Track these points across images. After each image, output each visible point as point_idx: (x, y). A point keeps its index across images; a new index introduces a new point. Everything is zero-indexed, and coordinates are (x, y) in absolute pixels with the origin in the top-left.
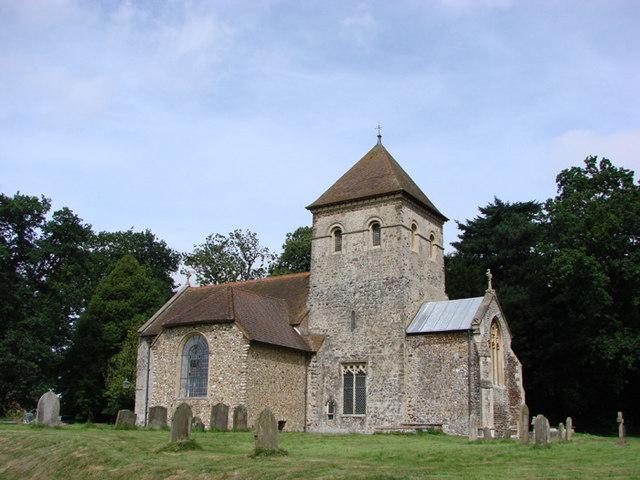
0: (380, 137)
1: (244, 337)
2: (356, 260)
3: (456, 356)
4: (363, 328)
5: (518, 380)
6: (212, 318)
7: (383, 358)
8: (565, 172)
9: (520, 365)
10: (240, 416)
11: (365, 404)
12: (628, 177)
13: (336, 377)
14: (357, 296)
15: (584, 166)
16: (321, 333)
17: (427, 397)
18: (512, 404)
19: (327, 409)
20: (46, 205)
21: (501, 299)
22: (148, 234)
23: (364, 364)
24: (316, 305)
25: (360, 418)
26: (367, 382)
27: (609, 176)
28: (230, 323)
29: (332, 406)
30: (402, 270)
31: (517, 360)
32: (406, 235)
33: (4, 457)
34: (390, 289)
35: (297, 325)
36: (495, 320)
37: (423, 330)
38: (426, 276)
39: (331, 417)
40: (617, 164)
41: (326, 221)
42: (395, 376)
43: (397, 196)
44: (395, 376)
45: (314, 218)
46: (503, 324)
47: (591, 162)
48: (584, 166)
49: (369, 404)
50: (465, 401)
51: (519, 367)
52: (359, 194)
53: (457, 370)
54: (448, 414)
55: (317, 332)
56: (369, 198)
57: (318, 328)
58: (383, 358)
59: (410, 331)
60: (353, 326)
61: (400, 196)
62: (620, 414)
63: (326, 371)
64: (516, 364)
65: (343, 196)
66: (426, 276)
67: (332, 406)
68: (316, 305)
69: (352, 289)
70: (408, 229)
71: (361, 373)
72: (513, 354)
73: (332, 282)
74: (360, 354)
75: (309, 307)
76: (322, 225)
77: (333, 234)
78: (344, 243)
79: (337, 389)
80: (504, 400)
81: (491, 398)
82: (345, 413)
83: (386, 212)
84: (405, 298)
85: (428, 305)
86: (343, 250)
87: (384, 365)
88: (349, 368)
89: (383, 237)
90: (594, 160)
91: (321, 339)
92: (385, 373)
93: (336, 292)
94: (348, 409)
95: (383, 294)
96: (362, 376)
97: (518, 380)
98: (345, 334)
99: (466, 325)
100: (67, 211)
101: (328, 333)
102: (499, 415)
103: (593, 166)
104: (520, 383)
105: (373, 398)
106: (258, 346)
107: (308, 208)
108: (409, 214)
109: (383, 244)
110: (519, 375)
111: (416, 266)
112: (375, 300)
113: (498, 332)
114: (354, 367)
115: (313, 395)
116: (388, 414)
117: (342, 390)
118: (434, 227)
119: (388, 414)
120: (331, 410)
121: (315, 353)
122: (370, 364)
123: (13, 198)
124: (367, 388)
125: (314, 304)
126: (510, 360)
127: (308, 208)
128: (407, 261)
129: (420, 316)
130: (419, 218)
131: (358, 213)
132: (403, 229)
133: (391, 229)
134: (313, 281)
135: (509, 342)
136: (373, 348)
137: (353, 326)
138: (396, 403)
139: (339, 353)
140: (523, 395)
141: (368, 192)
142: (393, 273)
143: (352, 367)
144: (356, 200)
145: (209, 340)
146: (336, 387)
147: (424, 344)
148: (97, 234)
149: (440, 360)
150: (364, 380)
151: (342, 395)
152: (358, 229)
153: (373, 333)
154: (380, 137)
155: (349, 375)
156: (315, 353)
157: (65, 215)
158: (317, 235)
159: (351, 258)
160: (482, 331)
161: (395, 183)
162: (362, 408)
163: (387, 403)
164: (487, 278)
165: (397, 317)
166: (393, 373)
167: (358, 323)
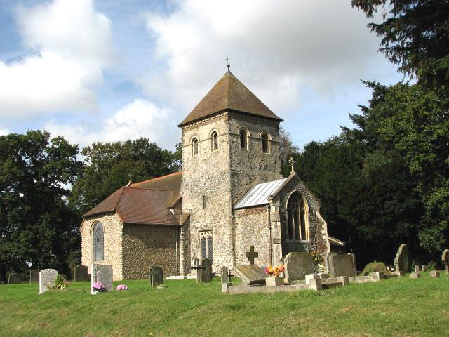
0: (228, 66)
2: (205, 160)
3: (262, 222)
4: (210, 206)
5: (324, 234)
7: (220, 226)
20: (48, 135)
28: (113, 213)
31: (323, 220)
33: (2, 305)
41: (189, 134)
52: (207, 113)
58: (220, 226)
60: (204, 206)
64: (323, 223)
89: (219, 143)
95: (220, 182)
96: (210, 238)
97: (324, 234)
98: (201, 211)
100: (60, 138)
107: (179, 126)
109: (219, 148)
122: (214, 231)
123: (25, 134)
125: (184, 193)
127: (179, 126)
134: (184, 177)
137: (204, 206)
139: (198, 225)
145: (104, 224)
147: (244, 215)
154: (228, 66)
155: (204, 239)
157: (59, 140)
158: (185, 144)
159: (203, 158)
163: (224, 257)
167: (207, 204)
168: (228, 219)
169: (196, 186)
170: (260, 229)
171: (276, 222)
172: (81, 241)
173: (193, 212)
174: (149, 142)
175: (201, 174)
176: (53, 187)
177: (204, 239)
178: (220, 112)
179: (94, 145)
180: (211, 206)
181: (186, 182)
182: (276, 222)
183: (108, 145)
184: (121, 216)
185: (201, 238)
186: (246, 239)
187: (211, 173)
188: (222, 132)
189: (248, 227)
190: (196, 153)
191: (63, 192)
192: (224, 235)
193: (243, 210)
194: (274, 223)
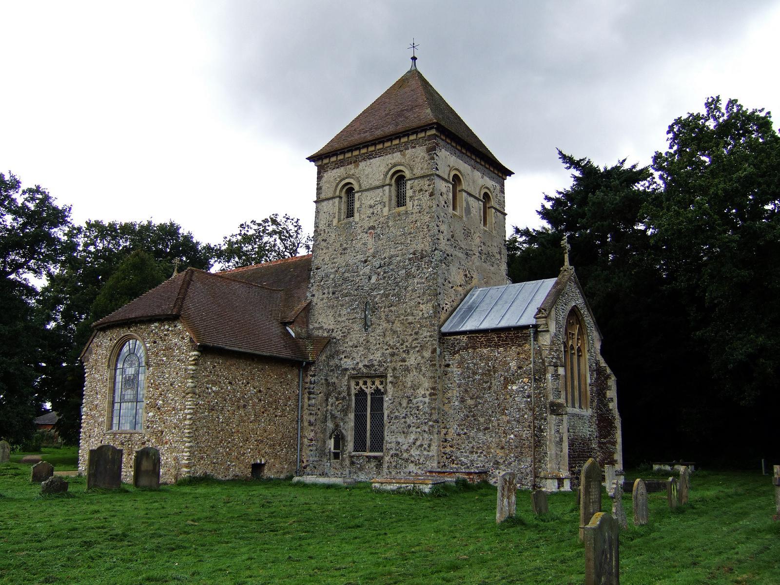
0: (414, 59)
1: (191, 340)
2: (373, 228)
3: (513, 365)
5: (612, 400)
6: (150, 313)
7: (407, 370)
8: (678, 121)
9: (613, 378)
10: (146, 465)
11: (382, 438)
12: (764, 124)
13: (344, 398)
14: (373, 280)
15: (704, 111)
16: (325, 334)
17: (470, 427)
18: (601, 436)
19: (331, 443)
21: (582, 280)
22: (172, 225)
23: (383, 376)
24: (318, 295)
25: (375, 457)
26: (385, 405)
27: (743, 123)
28: (172, 319)
29: (339, 440)
30: (435, 241)
31: (609, 371)
32: (444, 190)
34: (418, 268)
35: (290, 323)
36: (574, 313)
37: (464, 329)
38: (476, 250)
39: (336, 456)
40: (749, 105)
42: (424, 396)
43: (429, 133)
44: (424, 396)
45: (319, 173)
46: (588, 319)
47: (712, 104)
48: (704, 111)
49: (388, 437)
50: (526, 434)
51: (612, 382)
53: (514, 388)
54: (500, 453)
55: (320, 333)
56: (390, 138)
57: (321, 328)
58: (407, 370)
59: (444, 329)
61: (433, 132)
62: (763, 460)
63: (330, 389)
64: (608, 377)
65: (356, 138)
66: (476, 250)
67: (339, 440)
68: (318, 295)
69: (367, 270)
70: (478, 200)
71: (377, 391)
72: (603, 364)
73: (340, 261)
74: (376, 363)
75: (309, 297)
76: (329, 182)
77: (343, 194)
78: (357, 204)
79: (346, 415)
80: (588, 430)
81: (564, 428)
82: (356, 450)
83: (413, 158)
84: (440, 280)
85: (478, 292)
86: (356, 215)
87: (409, 380)
88: (377, 383)
89: (409, 193)
90: (718, 99)
91: (327, 343)
92: (409, 392)
93: (346, 275)
94: (360, 445)
95: (409, 275)
96: (378, 395)
98: (357, 335)
99: (528, 319)
101: (334, 335)
102: (578, 452)
103: (717, 109)
104: (613, 406)
105: (394, 427)
106: (205, 350)
107: (311, 159)
108: (448, 160)
110: (612, 393)
111: (459, 234)
112: (397, 284)
113: (581, 333)
114: (369, 384)
115: (310, 424)
116: (414, 452)
117: (352, 416)
118: (490, 183)
119: (414, 452)
120: (337, 446)
121: (313, 363)
122: (389, 379)
124: (386, 413)
126: (599, 371)
127: (311, 159)
128: (443, 228)
129: (464, 306)
130: (464, 167)
131: (376, 161)
132: (437, 181)
133: (421, 182)
135: (598, 345)
136: (393, 355)
138: (426, 435)
139: (348, 363)
140: (618, 423)
141: (390, 129)
142: (421, 244)
143: (365, 383)
144: (374, 142)
146: (345, 411)
147: (466, 348)
148: (107, 225)
149: (490, 373)
150: (381, 401)
151: (352, 424)
152: (377, 183)
153: (395, 332)
154: (414, 59)
155: (361, 394)
156: (313, 363)
159: (366, 225)
160: (553, 328)
161: (427, 114)
162: (378, 443)
163: (413, 437)
164: (564, 248)
165: (427, 309)
166: (421, 391)
168: (427, 354)
169: (345, 280)
170: (507, 382)
171: (556, 366)
172: (83, 380)
173: (338, 335)
174: (181, 231)
175: (360, 257)
176: (15, 283)
177: (361, 394)
178: (415, 131)
179: (88, 223)
180: (385, 325)
181: (320, 273)
182: (556, 366)
183: (112, 226)
184: (194, 329)
185: (353, 392)
186: (470, 402)
187: (387, 255)
188: (418, 172)
189: (475, 373)
190: (350, 213)
191: (31, 291)
192: (415, 387)
193: (464, 339)
194: (551, 369)
